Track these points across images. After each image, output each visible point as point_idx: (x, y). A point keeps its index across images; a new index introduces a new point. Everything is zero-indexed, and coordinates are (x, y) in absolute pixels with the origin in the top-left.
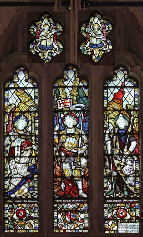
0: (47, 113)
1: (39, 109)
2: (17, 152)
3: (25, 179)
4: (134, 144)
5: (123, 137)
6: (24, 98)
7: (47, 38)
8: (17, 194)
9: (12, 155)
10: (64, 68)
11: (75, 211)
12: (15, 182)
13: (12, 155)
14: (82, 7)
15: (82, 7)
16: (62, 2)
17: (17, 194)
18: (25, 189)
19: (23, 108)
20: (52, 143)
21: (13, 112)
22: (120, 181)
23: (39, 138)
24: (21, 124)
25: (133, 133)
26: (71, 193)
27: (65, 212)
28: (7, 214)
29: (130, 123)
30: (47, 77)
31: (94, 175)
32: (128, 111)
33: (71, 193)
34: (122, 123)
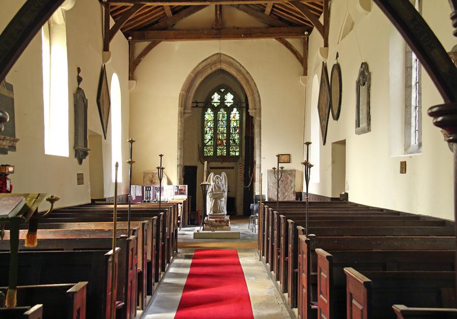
0: (216, 121)
1: (214, 120)
2: (208, 132)
3: (210, 140)
4: (238, 130)
5: (235, 128)
6: (210, 117)
7: (216, 97)
8: (208, 144)
9: (207, 133)
10: (217, 87)
11: (223, 149)
12: (207, 140)
13: (207, 133)
14: (105, 65)
15: (105, 65)
16: (383, 271)
17: (208, 144)
18: (210, 142)
19: (210, 120)
20: (217, 129)
21: (207, 121)
22: (234, 141)
23: (214, 128)
24: (209, 124)
25: (237, 127)
26: (222, 144)
27: (220, 149)
28: (205, 150)
29: (237, 124)
30: (216, 110)
31: (228, 139)
32: (237, 121)
33: (222, 144)
34: (235, 124)
